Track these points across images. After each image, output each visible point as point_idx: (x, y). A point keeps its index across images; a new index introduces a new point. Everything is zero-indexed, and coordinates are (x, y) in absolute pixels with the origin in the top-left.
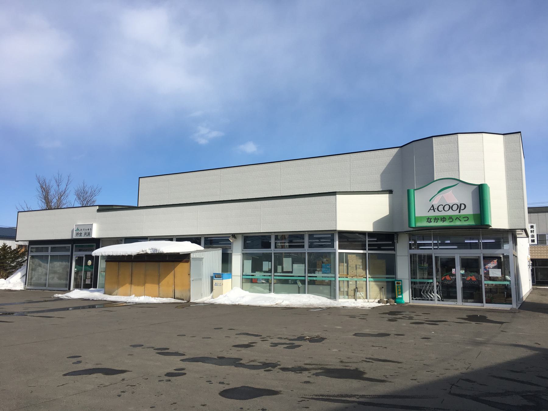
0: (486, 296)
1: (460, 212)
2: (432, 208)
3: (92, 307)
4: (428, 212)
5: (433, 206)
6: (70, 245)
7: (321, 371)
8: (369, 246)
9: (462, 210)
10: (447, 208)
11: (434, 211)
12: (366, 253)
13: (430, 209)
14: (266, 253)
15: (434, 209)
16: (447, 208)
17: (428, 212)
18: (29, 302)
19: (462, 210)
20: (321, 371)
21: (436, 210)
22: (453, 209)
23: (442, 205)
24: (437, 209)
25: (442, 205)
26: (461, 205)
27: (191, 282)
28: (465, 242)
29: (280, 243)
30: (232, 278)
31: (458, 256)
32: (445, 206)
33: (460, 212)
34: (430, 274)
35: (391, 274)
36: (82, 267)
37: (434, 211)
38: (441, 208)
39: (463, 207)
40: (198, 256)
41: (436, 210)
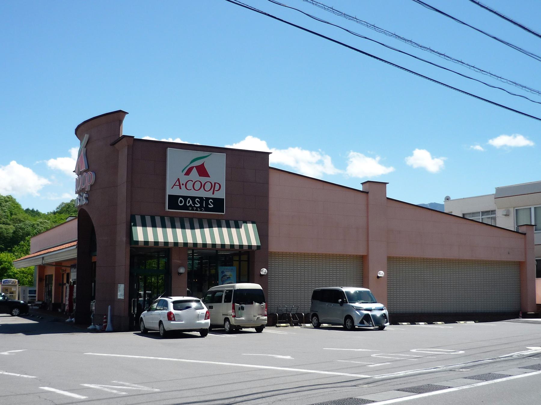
1: (213, 194)
2: (178, 183)
3: (24, 297)
5: (178, 179)
7: (244, 330)
9: (216, 191)
11: (180, 188)
13: (175, 185)
15: (180, 185)
19: (216, 191)
20: (244, 330)
21: (183, 187)
23: (192, 181)
24: (184, 184)
25: (192, 181)
27: (205, 313)
28: (151, 292)
29: (434, 317)
30: (229, 220)
33: (213, 194)
36: (211, 323)
37: (180, 188)
38: (190, 185)
39: (217, 187)
41: (183, 187)
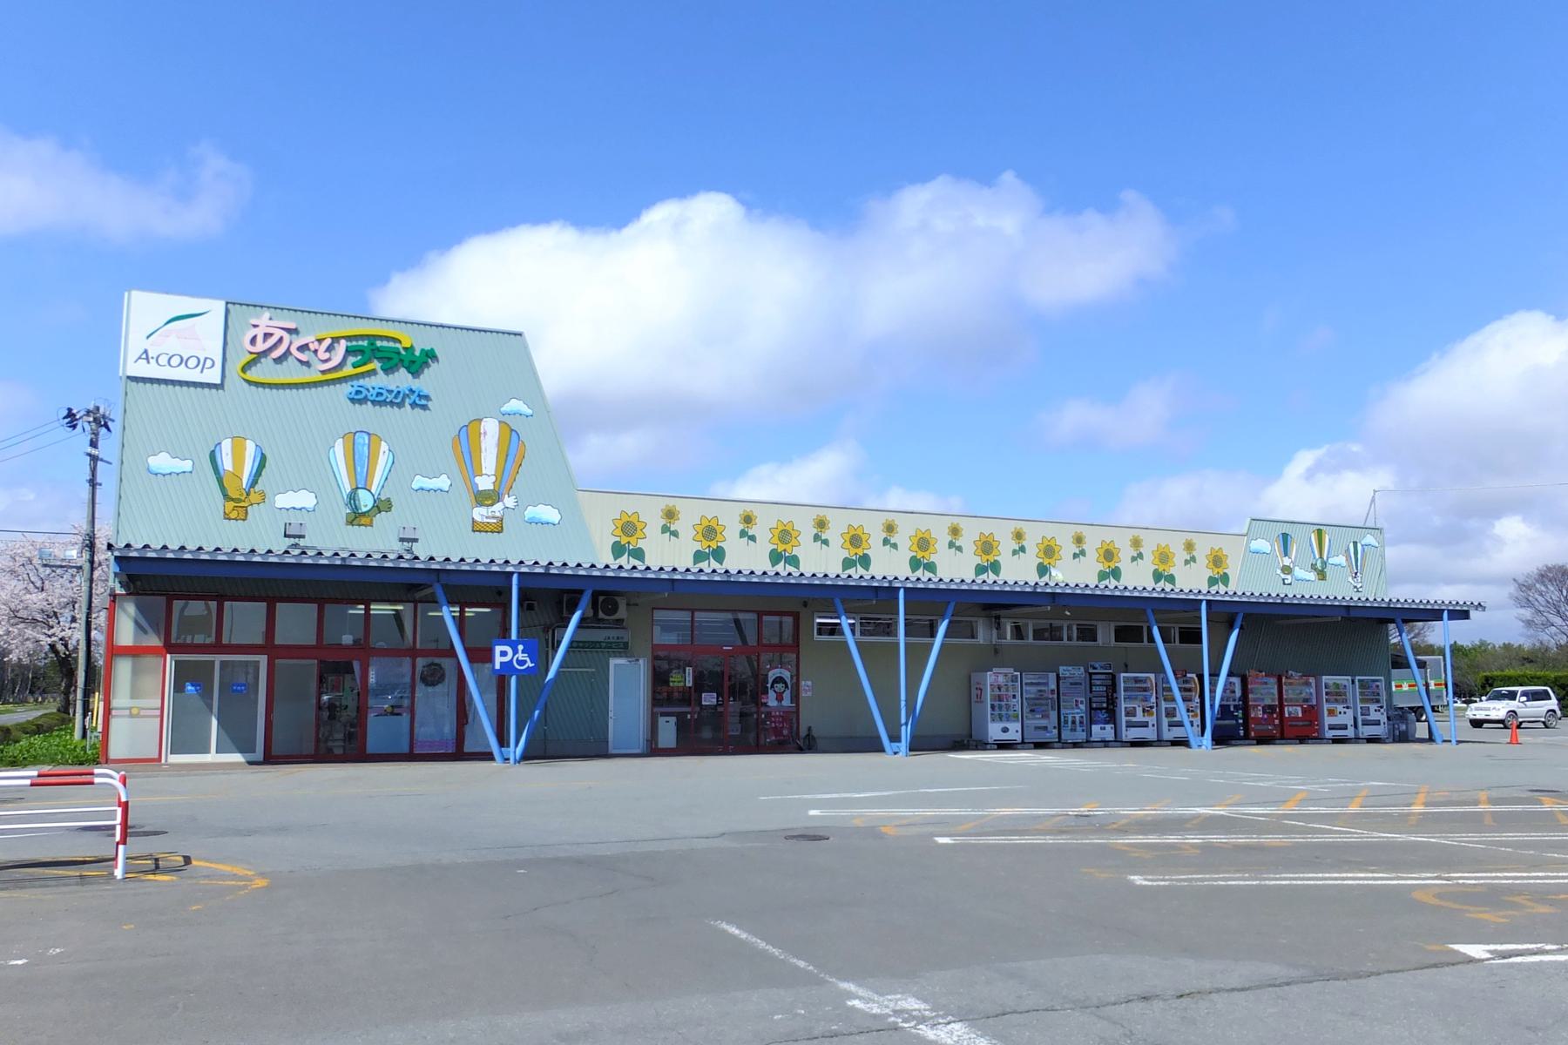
0: (1177, 678)
2: (144, 356)
4: (136, 362)
6: (1286, 709)
8: (1124, 691)
10: (175, 361)
11: (148, 362)
12: (217, 752)
13: (140, 358)
14: (866, 697)
15: (147, 359)
16: (175, 361)
17: (136, 362)
18: (1207, 848)
21: (153, 362)
22: (178, 357)
26: (206, 359)
31: (1177, 626)
32: (173, 356)
34: (1426, 804)
35: (1142, 633)
37: (148, 362)
39: (209, 363)
40: (1250, 703)
41: (153, 362)
